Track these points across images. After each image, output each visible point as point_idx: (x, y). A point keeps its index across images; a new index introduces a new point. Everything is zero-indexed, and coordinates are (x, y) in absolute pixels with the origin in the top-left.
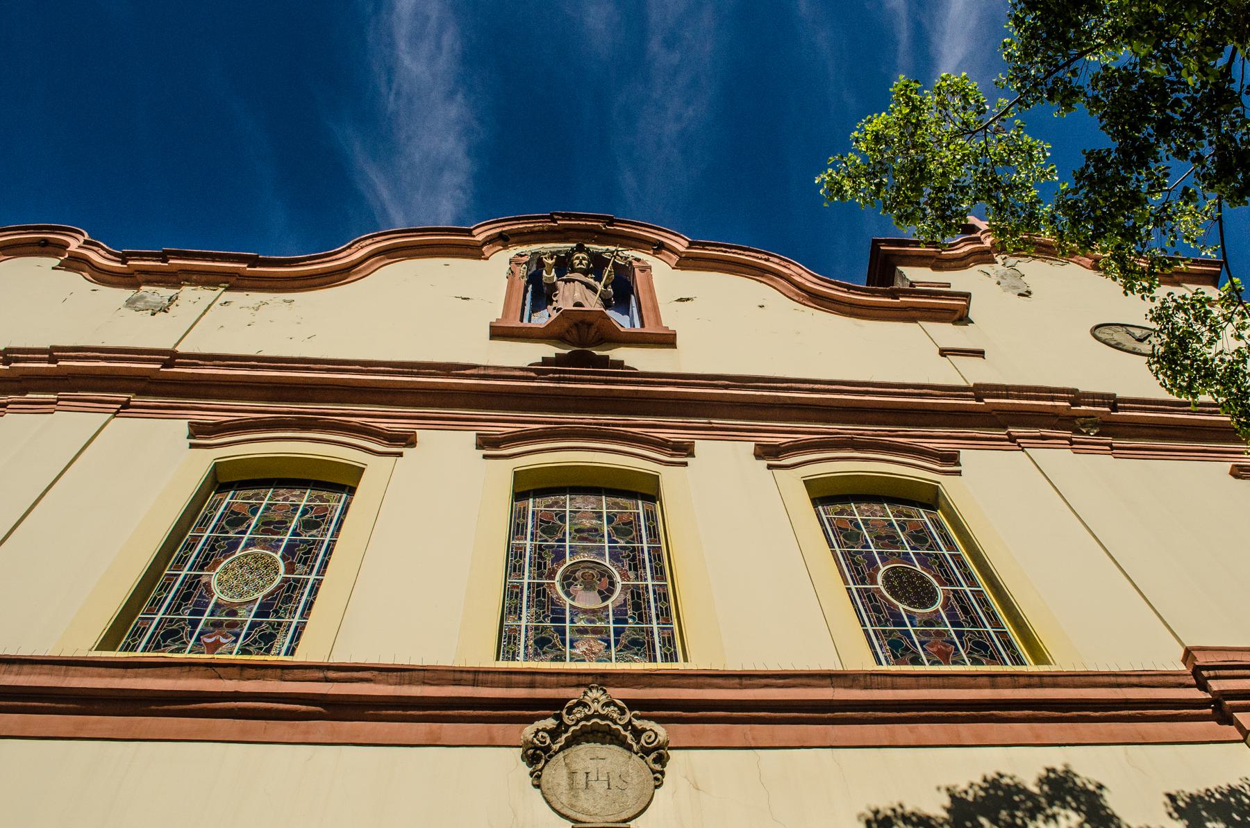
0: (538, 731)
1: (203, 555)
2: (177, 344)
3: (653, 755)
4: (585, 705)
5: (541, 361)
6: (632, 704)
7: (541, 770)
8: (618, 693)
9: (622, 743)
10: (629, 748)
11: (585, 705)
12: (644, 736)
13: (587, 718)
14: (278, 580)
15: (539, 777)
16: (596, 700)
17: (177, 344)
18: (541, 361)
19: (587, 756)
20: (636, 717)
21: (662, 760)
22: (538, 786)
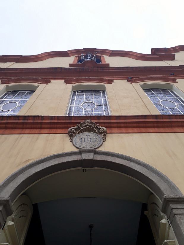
0: (72, 129)
1: (111, 78)
2: (25, 114)
3: (103, 134)
4: (85, 123)
5: (149, 52)
6: (97, 123)
7: (73, 138)
8: (93, 121)
9: (95, 132)
10: (96, 133)
11: (85, 123)
12: (100, 130)
13: (86, 126)
14: (96, 106)
15: (72, 140)
16: (88, 122)
17: (25, 114)
18: (149, 52)
19: (84, 135)
20: (98, 125)
21: (105, 135)
22: (71, 142)
